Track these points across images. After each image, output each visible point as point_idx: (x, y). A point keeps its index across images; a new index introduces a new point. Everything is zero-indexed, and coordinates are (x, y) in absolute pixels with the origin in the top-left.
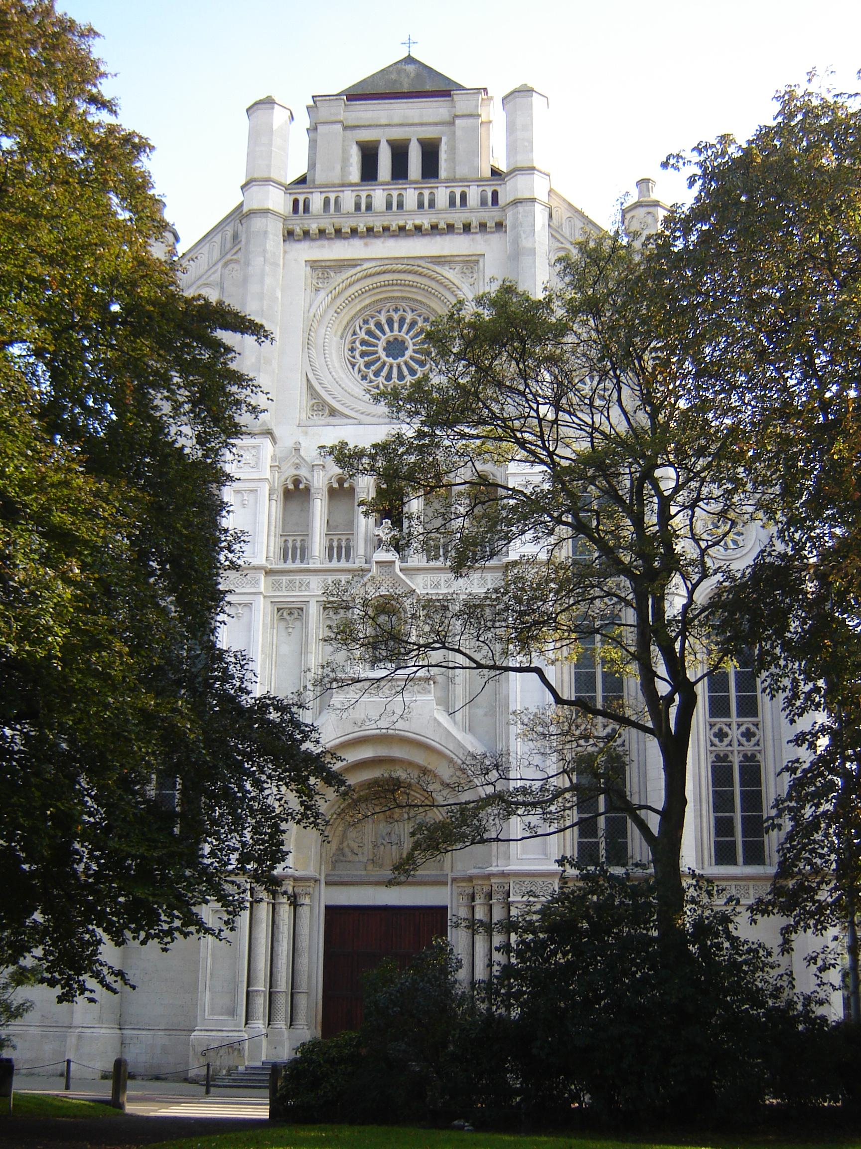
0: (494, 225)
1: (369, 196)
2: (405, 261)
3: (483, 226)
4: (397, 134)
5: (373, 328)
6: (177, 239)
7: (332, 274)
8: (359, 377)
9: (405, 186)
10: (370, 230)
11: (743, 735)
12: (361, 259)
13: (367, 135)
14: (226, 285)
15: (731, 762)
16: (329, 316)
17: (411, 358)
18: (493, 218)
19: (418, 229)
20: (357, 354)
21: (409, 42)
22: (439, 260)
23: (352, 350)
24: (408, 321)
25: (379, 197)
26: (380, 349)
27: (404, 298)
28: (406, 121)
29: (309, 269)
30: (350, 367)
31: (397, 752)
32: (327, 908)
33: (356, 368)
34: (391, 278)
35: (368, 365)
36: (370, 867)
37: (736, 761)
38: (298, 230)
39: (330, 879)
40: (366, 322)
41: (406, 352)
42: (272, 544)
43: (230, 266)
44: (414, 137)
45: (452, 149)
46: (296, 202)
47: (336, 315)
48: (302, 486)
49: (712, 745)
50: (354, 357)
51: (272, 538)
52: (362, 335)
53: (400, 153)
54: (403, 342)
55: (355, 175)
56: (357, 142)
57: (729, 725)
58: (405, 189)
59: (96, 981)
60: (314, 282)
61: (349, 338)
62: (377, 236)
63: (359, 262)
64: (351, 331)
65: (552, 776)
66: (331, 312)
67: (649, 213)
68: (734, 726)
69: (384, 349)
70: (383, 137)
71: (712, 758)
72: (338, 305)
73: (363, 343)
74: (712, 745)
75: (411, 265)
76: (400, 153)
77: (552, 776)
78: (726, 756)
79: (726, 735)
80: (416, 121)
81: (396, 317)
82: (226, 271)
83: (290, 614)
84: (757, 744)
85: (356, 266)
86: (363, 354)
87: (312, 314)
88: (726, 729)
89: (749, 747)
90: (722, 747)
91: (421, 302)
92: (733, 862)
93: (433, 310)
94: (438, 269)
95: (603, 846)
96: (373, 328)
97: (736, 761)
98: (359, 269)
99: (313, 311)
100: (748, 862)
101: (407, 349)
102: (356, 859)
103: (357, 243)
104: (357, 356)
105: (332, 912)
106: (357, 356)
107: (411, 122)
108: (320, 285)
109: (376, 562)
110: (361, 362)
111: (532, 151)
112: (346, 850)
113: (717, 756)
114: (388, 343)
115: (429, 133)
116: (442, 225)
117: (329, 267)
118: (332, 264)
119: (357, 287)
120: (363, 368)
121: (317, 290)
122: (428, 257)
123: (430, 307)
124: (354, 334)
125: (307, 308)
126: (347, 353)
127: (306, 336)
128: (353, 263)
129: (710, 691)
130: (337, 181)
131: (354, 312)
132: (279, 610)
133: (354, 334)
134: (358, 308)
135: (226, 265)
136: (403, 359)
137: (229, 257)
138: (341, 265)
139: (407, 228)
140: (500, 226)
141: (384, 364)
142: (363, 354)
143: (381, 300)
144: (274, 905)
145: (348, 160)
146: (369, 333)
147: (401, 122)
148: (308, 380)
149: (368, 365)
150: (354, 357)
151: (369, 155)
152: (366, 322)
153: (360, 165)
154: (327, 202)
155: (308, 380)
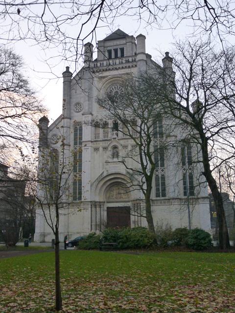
3: (132, 66)
4: (115, 47)
19: (119, 68)
21: (119, 26)
37: (160, 175)
38: (95, 71)
44: (118, 47)
45: (127, 50)
53: (116, 51)
59: (28, 86)
65: (135, 185)
70: (112, 48)
76: (116, 51)
77: (135, 185)
89: (163, 173)
92: (159, 197)
97: (160, 175)
100: (163, 196)
105: (108, 208)
128: (107, 76)
129: (193, 181)
140: (136, 66)
151: (110, 52)
154: (101, 64)
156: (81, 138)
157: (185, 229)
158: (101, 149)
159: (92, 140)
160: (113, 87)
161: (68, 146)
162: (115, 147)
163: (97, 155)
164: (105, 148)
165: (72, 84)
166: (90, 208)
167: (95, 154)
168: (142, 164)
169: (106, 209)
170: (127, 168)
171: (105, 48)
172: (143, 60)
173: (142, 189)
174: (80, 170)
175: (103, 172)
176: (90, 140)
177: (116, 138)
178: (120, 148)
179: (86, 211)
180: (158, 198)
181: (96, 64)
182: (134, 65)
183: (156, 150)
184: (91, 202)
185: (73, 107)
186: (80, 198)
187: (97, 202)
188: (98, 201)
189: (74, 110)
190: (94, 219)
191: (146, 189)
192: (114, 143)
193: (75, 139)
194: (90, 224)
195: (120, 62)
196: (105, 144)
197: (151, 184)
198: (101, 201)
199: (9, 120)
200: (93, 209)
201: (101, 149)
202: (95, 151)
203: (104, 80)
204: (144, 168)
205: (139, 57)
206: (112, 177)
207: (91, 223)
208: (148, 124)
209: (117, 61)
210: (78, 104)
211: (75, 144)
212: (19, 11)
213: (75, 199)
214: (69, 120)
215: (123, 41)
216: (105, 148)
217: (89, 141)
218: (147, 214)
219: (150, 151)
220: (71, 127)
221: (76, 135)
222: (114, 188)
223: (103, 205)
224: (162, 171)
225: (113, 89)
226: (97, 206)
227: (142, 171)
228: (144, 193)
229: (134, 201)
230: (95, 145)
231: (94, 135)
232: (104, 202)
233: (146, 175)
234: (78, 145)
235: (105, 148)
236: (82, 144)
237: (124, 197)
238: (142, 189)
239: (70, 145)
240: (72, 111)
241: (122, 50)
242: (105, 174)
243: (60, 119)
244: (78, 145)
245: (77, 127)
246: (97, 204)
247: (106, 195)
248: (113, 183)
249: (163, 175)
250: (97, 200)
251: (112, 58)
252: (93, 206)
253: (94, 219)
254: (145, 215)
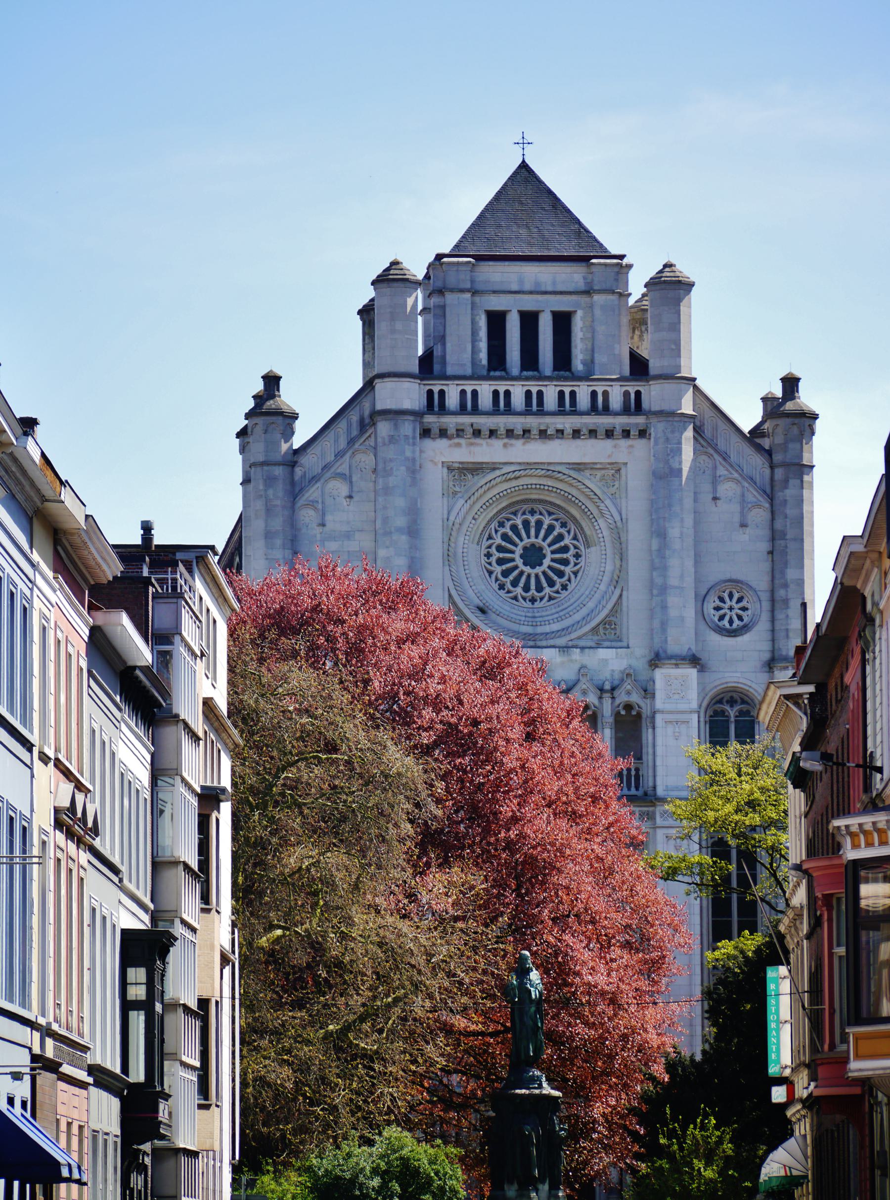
0: (637, 433)
1: (638, 394)
2: (546, 467)
4: (529, 303)
7: (470, 476)
8: (496, 586)
9: (545, 383)
12: (500, 463)
13: (497, 303)
14: (354, 479)
15: (727, 716)
16: (467, 523)
17: (549, 567)
18: (637, 424)
19: (560, 432)
22: (579, 467)
23: (488, 555)
26: (517, 556)
27: (541, 501)
28: (538, 289)
29: (445, 470)
30: (487, 575)
32: (199, 999)
33: (493, 576)
34: (530, 482)
40: (501, 524)
41: (544, 561)
46: (430, 393)
47: (473, 521)
50: (490, 564)
53: (529, 320)
54: (541, 549)
58: (546, 386)
60: (451, 486)
61: (485, 544)
63: (498, 466)
67: (794, 424)
69: (521, 556)
72: (476, 510)
76: (529, 320)
80: (550, 289)
85: (494, 469)
87: (451, 523)
91: (559, 506)
93: (572, 516)
98: (498, 473)
101: (544, 556)
103: (497, 444)
104: (494, 563)
106: (494, 563)
107: (543, 289)
108: (457, 489)
111: (679, 356)
115: (562, 304)
117: (467, 469)
118: (470, 466)
120: (500, 576)
121: (455, 493)
122: (569, 464)
123: (568, 512)
124: (490, 537)
125: (445, 516)
126: (484, 559)
127: (446, 547)
131: (491, 514)
134: (495, 511)
136: (523, 543)
139: (549, 433)
140: (643, 433)
141: (522, 573)
142: (500, 562)
145: (478, 335)
147: (533, 289)
148: (450, 596)
149: (505, 574)
150: (490, 564)
151: (496, 320)
155: (450, 596)
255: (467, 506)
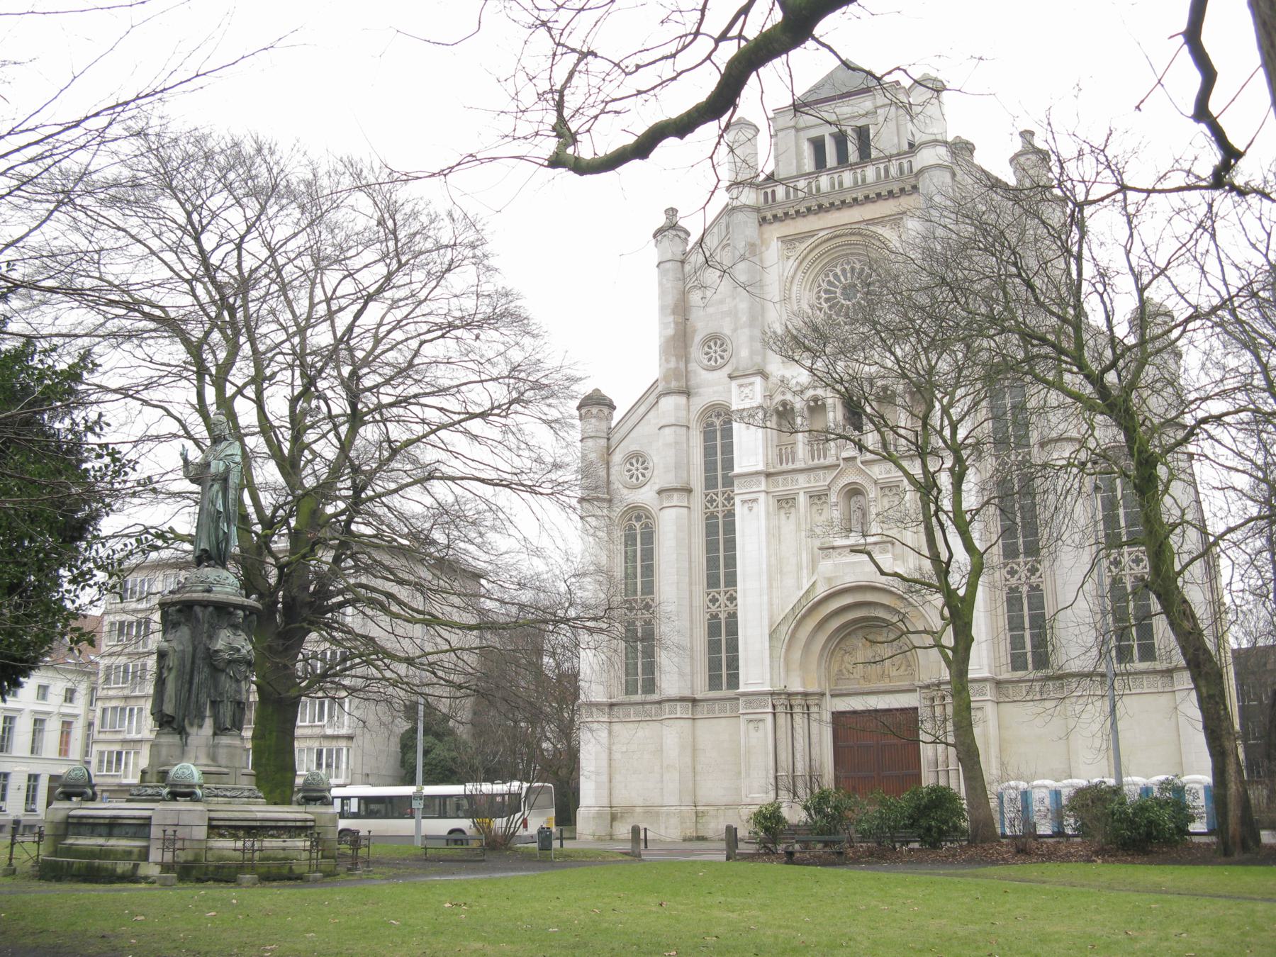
5: (832, 279)
6: (688, 234)
10: (855, 200)
11: (717, 600)
20: (822, 301)
24: (839, 273)
25: (824, 181)
31: (869, 597)
35: (830, 308)
36: (862, 681)
37: (722, 616)
39: (833, 692)
42: (770, 453)
43: (726, 250)
48: (788, 407)
49: (708, 608)
51: (770, 449)
52: (824, 285)
55: (809, 164)
56: (808, 139)
57: (719, 593)
61: (816, 290)
62: (827, 210)
64: (817, 284)
66: (800, 273)
68: (1126, 555)
71: (708, 616)
73: (826, 291)
74: (708, 608)
75: (854, 231)
76: (841, 140)
78: (717, 615)
79: (717, 600)
81: (848, 268)
82: (724, 253)
83: (787, 503)
84: (1041, 577)
85: (813, 236)
86: (827, 300)
88: (717, 596)
90: (714, 609)
94: (873, 228)
95: (1029, 655)
96: (832, 279)
97: (722, 616)
98: (816, 238)
99: (785, 274)
100: (1142, 659)
102: (852, 676)
103: (812, 218)
105: (838, 717)
109: (844, 459)
110: (825, 306)
112: (844, 671)
113: (1010, 589)
114: (844, 288)
116: (872, 195)
119: (816, 251)
121: (788, 258)
128: (811, 234)
130: (795, 174)
132: (778, 501)
133: (820, 286)
135: (724, 248)
137: (725, 242)
138: (802, 237)
143: (835, 258)
144: (792, 714)
146: (829, 283)
152: (827, 275)
153: (813, 157)
156: (729, 464)
157: (576, 696)
158: (802, 499)
159: (772, 470)
160: (838, 271)
161: (685, 494)
162: (854, 492)
163: (788, 526)
164: (819, 497)
165: (687, 267)
166: (769, 718)
167: (783, 516)
168: (935, 558)
169: (827, 717)
170: (883, 573)
171: (801, 134)
172: (939, 166)
173: (941, 647)
174: (732, 580)
175: (814, 584)
176: (761, 467)
177: (854, 458)
178: (872, 493)
179: (757, 729)
180: (1020, 674)
181: (769, 191)
182: (908, 188)
183: (516, 657)
184: (772, 694)
185: (696, 352)
186: (734, 681)
187: (797, 694)
188: (801, 689)
189: (699, 363)
190: (784, 756)
191: (952, 644)
192: (851, 477)
193: (710, 466)
194: (772, 772)
195: (856, 182)
196: (821, 481)
197: (968, 625)
198: (810, 690)
199: (475, 426)
200: (782, 719)
201: (802, 499)
202: (780, 508)
203: (802, 247)
204: (942, 569)
205: (926, 157)
206: (859, 598)
207: (776, 771)
208: (952, 411)
209: (848, 178)
210: (714, 339)
211: (710, 483)
212: (477, 337)
213: (714, 683)
214: (682, 400)
215: (865, 104)
216: (818, 497)
217: (757, 473)
218: (956, 736)
219: (965, 506)
220: (693, 425)
221: (709, 451)
222: (858, 641)
223: (819, 706)
224: (1033, 570)
225: (836, 276)
226: (796, 710)
227: (935, 581)
228: (945, 657)
229: (928, 687)
230: (781, 486)
231: (776, 451)
232: (823, 695)
233: (949, 594)
234: (720, 489)
235: (819, 497)
236: (732, 484)
237: (894, 673)
238: (941, 647)
239: (689, 491)
240: (693, 366)
241: (863, 133)
242: (821, 591)
243: (652, 399)
244: (720, 489)
245: (712, 424)
246: (797, 701)
247: (828, 669)
248: (855, 621)
249: (1035, 588)
250: (796, 687)
251: (828, 166)
252: (779, 709)
253: (784, 756)
254: (951, 739)
255: (796, 264)
